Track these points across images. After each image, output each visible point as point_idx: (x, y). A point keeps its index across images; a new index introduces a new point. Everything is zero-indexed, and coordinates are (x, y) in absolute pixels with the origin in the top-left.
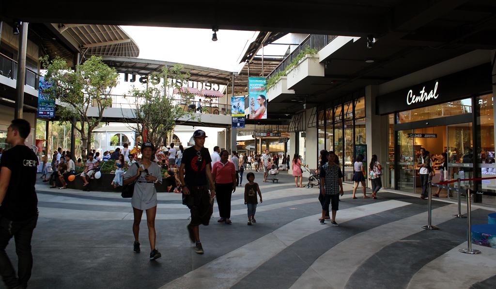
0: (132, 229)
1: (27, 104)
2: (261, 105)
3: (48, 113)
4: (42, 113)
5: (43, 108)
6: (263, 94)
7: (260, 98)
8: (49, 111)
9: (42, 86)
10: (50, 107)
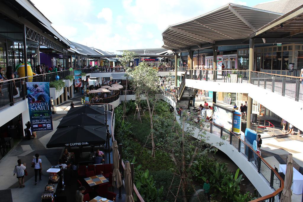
0: (17, 162)
1: (176, 200)
2: (80, 82)
3: (44, 125)
4: (37, 126)
5: (36, 121)
6: (80, 77)
7: (79, 79)
8: (45, 123)
9: (31, 94)
10: (45, 119)
